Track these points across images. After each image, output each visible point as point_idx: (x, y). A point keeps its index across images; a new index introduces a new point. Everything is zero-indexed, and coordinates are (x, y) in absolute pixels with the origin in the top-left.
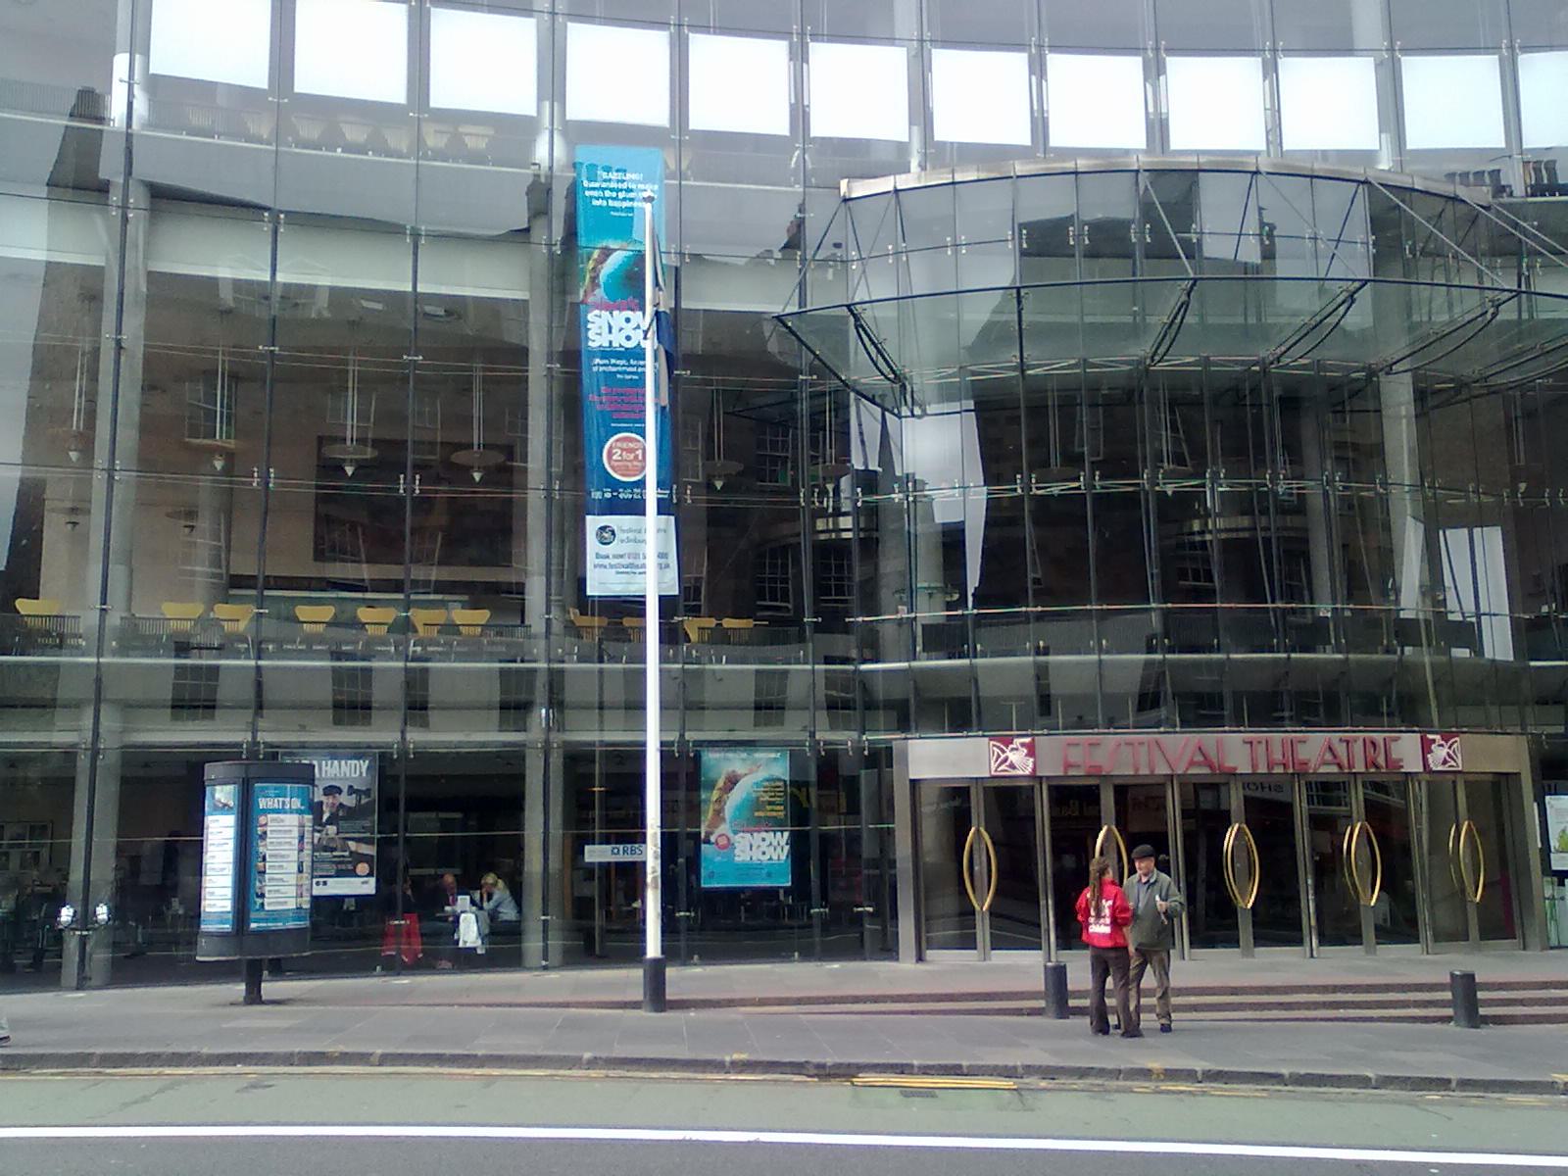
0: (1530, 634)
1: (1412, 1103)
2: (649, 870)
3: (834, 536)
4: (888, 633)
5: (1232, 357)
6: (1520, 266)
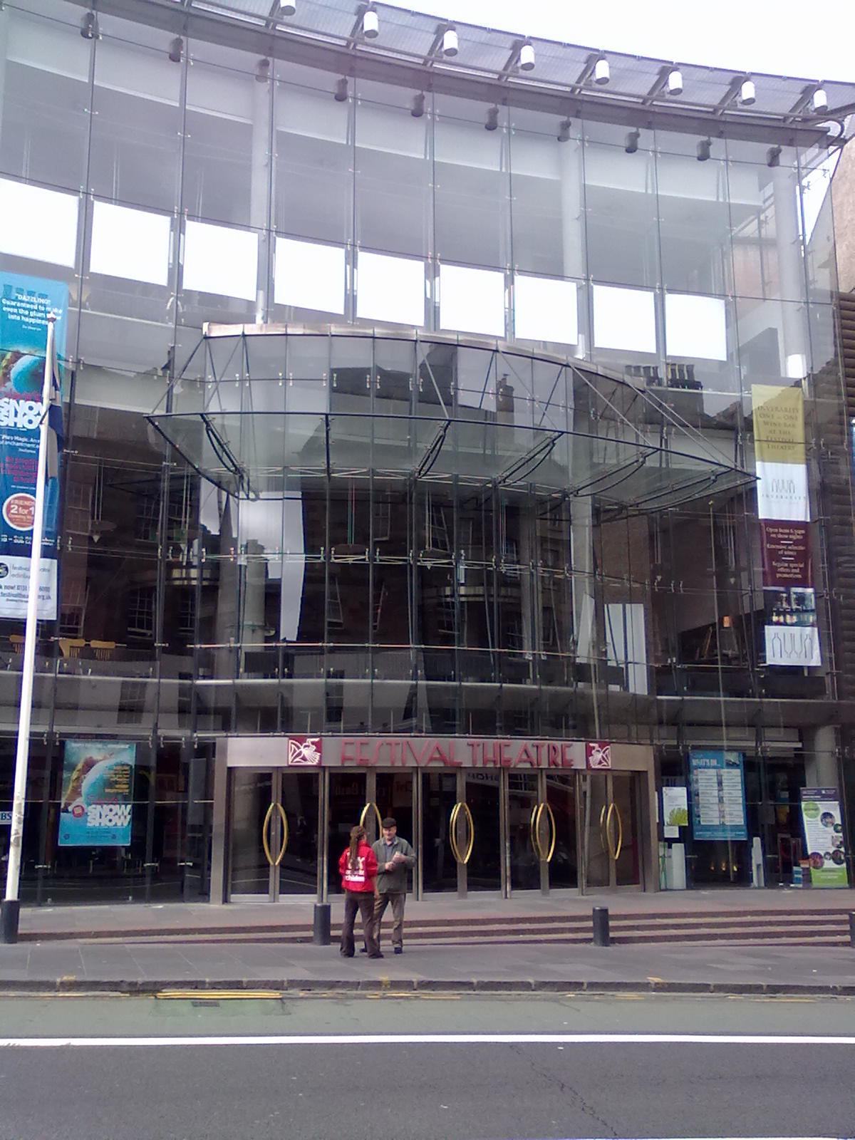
0: (659, 678)
1: (556, 1000)
2: (13, 832)
3: (186, 582)
4: (223, 659)
5: (476, 477)
6: (662, 432)
